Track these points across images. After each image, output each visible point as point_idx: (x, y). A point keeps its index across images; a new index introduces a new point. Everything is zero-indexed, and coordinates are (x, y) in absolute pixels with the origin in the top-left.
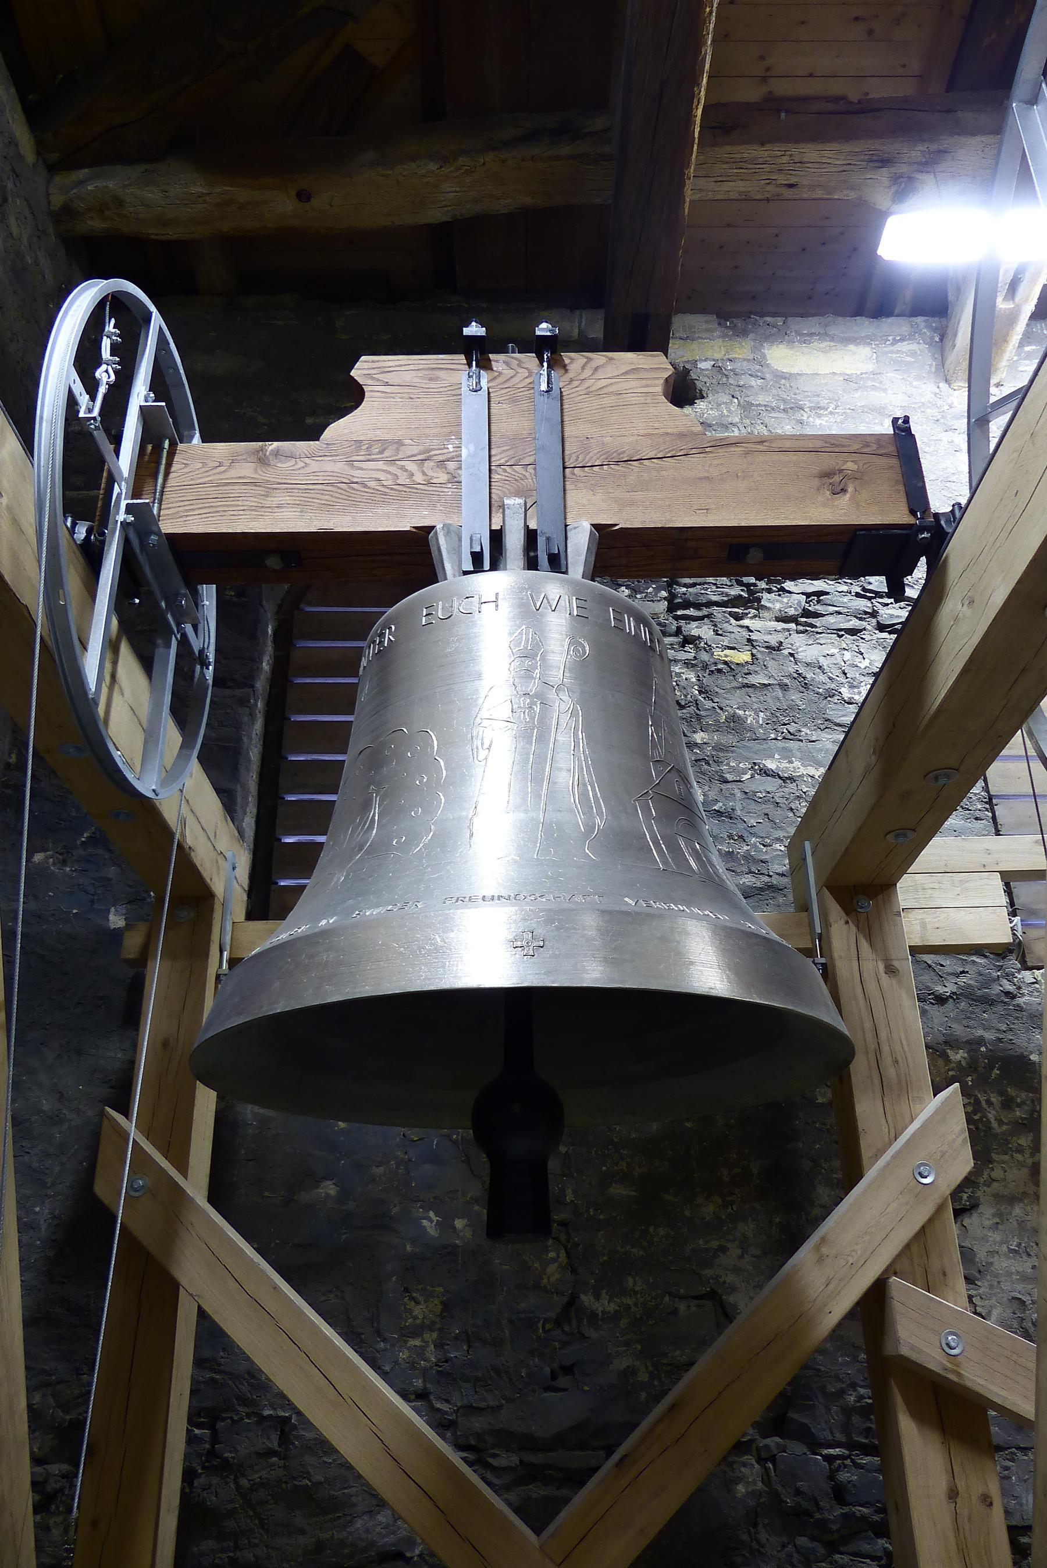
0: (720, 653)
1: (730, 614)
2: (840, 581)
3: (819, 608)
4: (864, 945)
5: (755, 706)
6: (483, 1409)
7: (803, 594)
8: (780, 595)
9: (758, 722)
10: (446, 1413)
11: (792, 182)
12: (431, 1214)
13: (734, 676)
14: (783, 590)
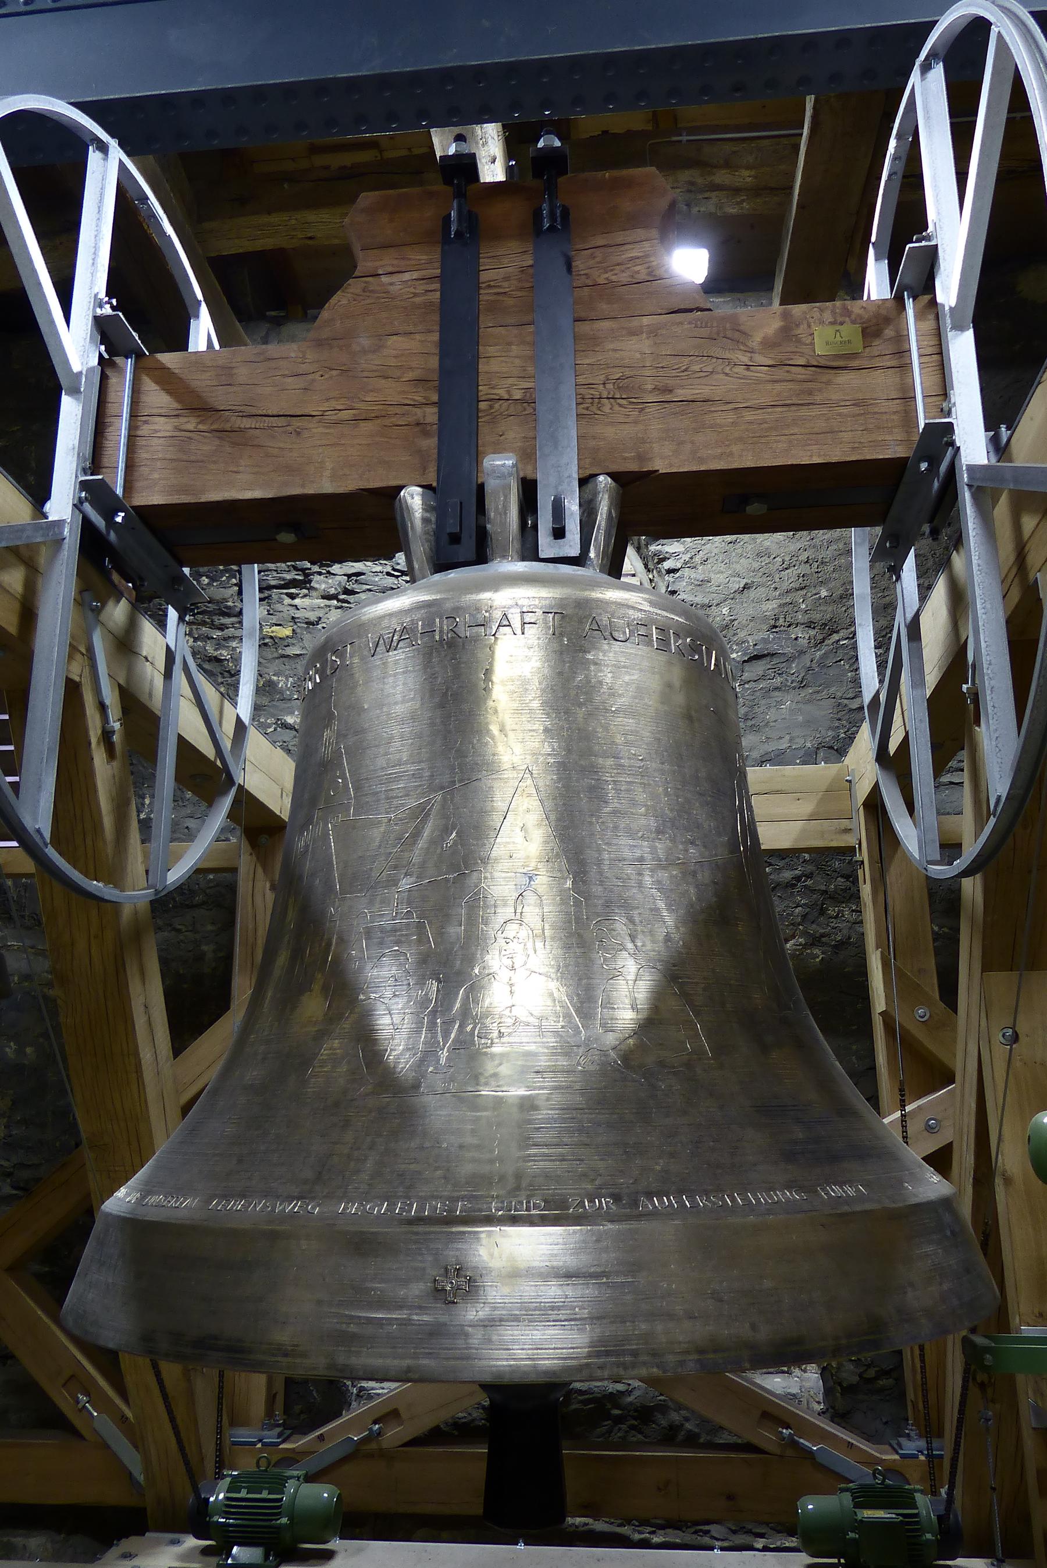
0: (268, 630)
1: (287, 594)
2: (377, 562)
3: (357, 587)
4: (260, 870)
5: (287, 672)
6: (29, 1166)
7: (344, 575)
8: (327, 577)
9: (287, 685)
10: (6, 1167)
11: (309, 235)
12: (12, 1044)
13: (276, 648)
14: (329, 572)
